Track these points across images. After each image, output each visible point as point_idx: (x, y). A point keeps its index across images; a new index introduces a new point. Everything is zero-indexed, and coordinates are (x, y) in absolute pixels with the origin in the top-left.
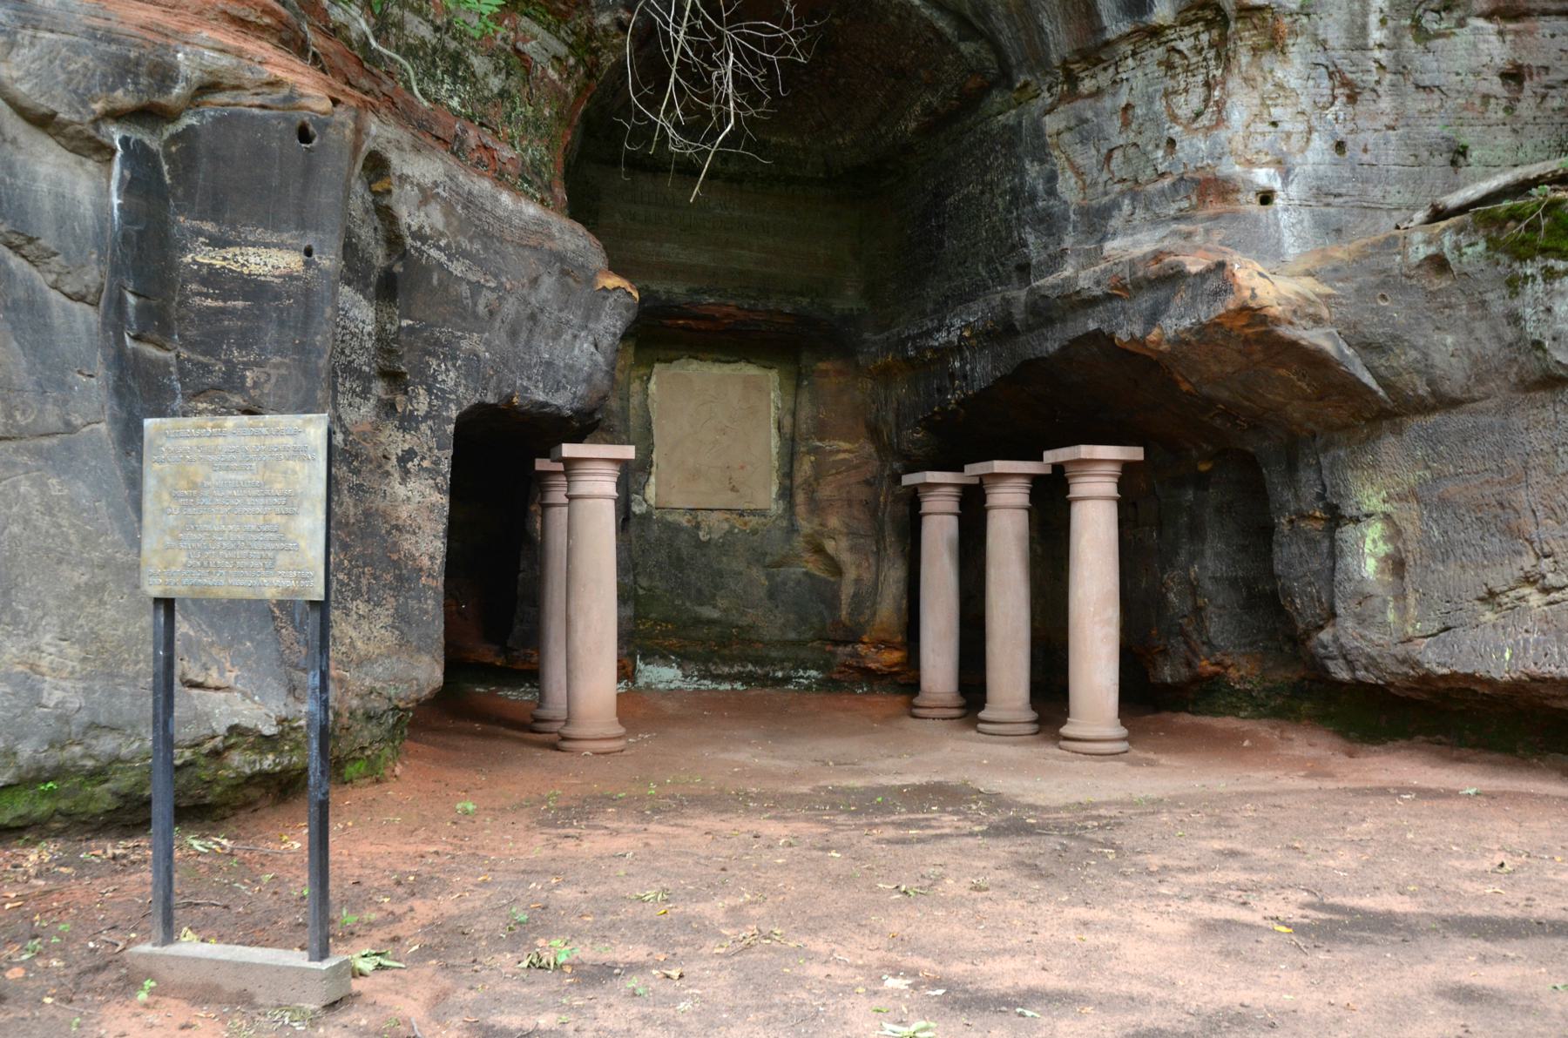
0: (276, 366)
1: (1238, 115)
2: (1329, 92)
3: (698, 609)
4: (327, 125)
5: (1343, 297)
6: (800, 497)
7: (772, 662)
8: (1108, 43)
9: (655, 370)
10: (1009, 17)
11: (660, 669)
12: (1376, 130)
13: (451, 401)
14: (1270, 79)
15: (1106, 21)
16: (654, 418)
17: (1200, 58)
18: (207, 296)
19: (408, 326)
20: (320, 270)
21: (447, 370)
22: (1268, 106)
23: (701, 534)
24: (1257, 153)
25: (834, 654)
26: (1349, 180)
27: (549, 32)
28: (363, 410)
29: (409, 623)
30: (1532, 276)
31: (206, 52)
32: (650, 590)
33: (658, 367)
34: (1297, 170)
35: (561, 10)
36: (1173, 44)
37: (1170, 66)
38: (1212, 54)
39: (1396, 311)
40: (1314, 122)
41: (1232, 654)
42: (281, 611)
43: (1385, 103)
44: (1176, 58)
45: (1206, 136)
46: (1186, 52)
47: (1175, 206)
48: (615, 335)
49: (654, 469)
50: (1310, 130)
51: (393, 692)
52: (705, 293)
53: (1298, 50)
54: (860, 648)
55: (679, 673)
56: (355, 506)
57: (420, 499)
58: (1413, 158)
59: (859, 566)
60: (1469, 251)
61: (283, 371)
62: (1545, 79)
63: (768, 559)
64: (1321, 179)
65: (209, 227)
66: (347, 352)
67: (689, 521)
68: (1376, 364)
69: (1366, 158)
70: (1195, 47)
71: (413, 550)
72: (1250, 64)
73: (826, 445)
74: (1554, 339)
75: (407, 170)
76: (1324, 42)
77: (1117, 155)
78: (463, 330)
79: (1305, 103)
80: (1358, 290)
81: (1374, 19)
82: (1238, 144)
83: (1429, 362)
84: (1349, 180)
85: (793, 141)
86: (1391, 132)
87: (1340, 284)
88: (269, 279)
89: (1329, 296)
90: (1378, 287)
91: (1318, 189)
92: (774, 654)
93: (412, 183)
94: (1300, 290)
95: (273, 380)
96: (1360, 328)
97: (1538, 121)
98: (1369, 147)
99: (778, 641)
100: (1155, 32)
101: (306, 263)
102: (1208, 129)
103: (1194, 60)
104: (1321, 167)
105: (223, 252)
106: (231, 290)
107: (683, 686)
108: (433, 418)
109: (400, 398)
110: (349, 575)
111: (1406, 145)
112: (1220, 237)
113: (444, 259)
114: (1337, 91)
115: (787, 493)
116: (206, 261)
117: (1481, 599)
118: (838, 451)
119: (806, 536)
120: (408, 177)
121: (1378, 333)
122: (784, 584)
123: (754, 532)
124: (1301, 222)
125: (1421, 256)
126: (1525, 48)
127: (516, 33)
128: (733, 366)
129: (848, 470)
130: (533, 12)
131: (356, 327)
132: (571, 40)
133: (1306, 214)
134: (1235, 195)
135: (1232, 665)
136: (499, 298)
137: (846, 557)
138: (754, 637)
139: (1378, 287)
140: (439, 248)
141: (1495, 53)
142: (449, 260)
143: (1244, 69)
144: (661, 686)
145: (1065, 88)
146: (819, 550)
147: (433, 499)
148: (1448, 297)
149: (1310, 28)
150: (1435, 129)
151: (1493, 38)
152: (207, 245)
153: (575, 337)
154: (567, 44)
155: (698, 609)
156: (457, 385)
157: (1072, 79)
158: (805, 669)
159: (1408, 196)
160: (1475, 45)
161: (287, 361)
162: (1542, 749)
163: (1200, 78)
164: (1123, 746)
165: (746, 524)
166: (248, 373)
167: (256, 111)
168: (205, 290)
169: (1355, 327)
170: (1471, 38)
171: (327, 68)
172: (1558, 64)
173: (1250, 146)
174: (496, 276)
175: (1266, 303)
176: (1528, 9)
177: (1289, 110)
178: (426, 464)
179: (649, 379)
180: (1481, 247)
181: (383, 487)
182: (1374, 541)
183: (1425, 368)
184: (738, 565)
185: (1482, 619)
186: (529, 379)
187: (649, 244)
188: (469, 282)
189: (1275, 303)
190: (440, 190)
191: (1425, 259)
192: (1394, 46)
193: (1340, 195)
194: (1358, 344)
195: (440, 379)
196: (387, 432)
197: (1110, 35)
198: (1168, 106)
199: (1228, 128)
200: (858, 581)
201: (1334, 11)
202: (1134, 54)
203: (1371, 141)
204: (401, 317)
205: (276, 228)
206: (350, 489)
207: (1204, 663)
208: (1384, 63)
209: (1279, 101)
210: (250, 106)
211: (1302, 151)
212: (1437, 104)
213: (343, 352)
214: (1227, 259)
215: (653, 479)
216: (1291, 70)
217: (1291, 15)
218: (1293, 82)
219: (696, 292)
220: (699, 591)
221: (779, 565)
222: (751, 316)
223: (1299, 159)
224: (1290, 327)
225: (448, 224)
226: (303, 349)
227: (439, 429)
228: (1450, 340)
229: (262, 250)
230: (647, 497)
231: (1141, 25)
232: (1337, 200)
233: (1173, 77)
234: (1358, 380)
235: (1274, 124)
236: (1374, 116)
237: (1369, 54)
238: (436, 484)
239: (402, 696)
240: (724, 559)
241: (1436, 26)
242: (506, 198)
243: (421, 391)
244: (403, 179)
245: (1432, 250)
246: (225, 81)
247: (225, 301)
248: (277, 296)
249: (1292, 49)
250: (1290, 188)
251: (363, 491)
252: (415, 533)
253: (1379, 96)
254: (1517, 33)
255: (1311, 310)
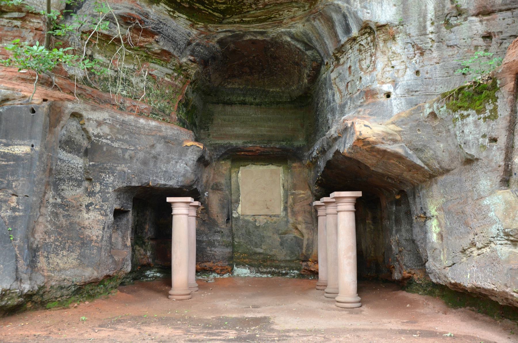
0: (22, 181)
1: (380, 66)
2: (413, 53)
3: (256, 249)
4: (39, 107)
5: (405, 131)
6: (289, 210)
7: (281, 267)
8: (343, 45)
9: (240, 169)
10: (317, 40)
11: (242, 270)
12: (431, 65)
13: (109, 186)
14: (390, 51)
15: (341, 38)
16: (240, 185)
17: (369, 47)
18: (3, 161)
19: (93, 164)
20: (35, 151)
21: (109, 177)
22: (391, 61)
23: (257, 223)
24: (386, 79)
25: (301, 265)
26: (420, 85)
27: (163, 66)
28: (78, 191)
29: (85, 258)
30: (458, 118)
31: (2, 90)
32: (239, 243)
33: (241, 168)
34: (400, 84)
35: (165, 60)
36: (360, 42)
37: (360, 51)
38: (371, 44)
39: (423, 135)
40: (408, 65)
41: (414, 269)
42: (20, 255)
43: (435, 54)
44: (362, 48)
45: (370, 75)
46: (364, 45)
47: (360, 101)
48: (194, 160)
49: (240, 202)
50: (406, 68)
51: (74, 280)
52: (249, 143)
53: (400, 38)
54: (309, 263)
55: (249, 271)
56: (66, 221)
57: (94, 218)
58: (446, 74)
59: (308, 234)
60: (442, 109)
61: (24, 182)
62: (501, 36)
63: (280, 232)
64: (409, 86)
65: (4, 141)
66: (70, 173)
67: (253, 219)
68: (421, 157)
69: (427, 76)
70: (367, 43)
71: (90, 234)
72: (383, 46)
73: (296, 192)
74: (465, 144)
75: (90, 116)
76: (409, 34)
77: (349, 84)
78: (118, 164)
79: (404, 58)
80: (410, 128)
81: (428, 23)
82: (379, 77)
83: (436, 155)
84: (420, 85)
85: (278, 90)
86: (437, 65)
87: (404, 126)
88: (21, 155)
89: (400, 131)
90: (416, 126)
91: (408, 90)
92: (282, 265)
93: (93, 120)
94: (384, 130)
95: (21, 185)
96: (412, 143)
97: (498, 53)
98: (428, 72)
99: (284, 260)
100: (354, 39)
101: (32, 150)
102: (371, 72)
103: (367, 47)
104: (410, 81)
105: (8, 148)
106: (10, 159)
107: (250, 275)
108: (101, 192)
109: (91, 186)
110: (61, 243)
111: (444, 69)
112: (368, 112)
113: (109, 142)
114: (416, 52)
115: (285, 209)
116: (3, 151)
117: (461, 252)
118: (300, 194)
119: (292, 224)
120: (91, 118)
121: (419, 145)
122: (287, 240)
123: (275, 223)
124: (401, 103)
125: (428, 113)
126: (491, 25)
127: (149, 68)
128: (267, 166)
129: (304, 200)
130: (155, 61)
131: (75, 165)
132: (173, 68)
133: (403, 100)
134: (376, 96)
135: (414, 273)
136: (135, 152)
137: (304, 231)
138: (275, 259)
139: (416, 126)
140: (107, 139)
141: (479, 29)
142: (112, 142)
143: (381, 48)
144: (242, 275)
145: (336, 62)
146: (297, 228)
147: (99, 218)
148: (439, 128)
149: (404, 30)
150: (455, 62)
151: (478, 23)
152: (3, 146)
153: (177, 162)
154: (172, 69)
155: (256, 249)
156: (113, 181)
157: (338, 59)
158: (293, 270)
159: (445, 88)
160: (470, 27)
161: (25, 179)
162: (503, 317)
163: (369, 53)
164: (359, 304)
165: (272, 220)
166: (13, 183)
167: (19, 106)
168: (2, 159)
169: (411, 143)
170: (469, 25)
171: (60, 89)
172: (506, 30)
173: (384, 76)
174: (134, 146)
175: (366, 136)
176: (493, 10)
177: (398, 61)
178: (97, 207)
179: (238, 172)
180: (445, 108)
181: (79, 215)
182: (435, 226)
183: (435, 157)
184: (270, 234)
185: (462, 260)
186: (156, 177)
187: (230, 128)
188: (121, 149)
189: (372, 136)
190: (108, 121)
191: (429, 114)
192: (438, 32)
193: (417, 91)
194: (413, 149)
195: (106, 180)
196: (83, 198)
197: (342, 42)
198: (360, 65)
199: (376, 71)
200: (308, 239)
201: (413, 22)
202: (351, 48)
203: (429, 69)
204: (90, 161)
205: (23, 140)
206: (63, 216)
207: (405, 272)
208: (434, 39)
209: (394, 58)
210: (18, 104)
211: (403, 76)
212: (456, 52)
213: (68, 174)
214: (437, 120)
215: (240, 205)
216: (398, 47)
217: (396, 26)
218: (399, 51)
219: (246, 143)
220: (256, 243)
221: (285, 233)
222: (266, 149)
223: (401, 79)
224: (382, 145)
225: (111, 131)
226: (29, 175)
227: (104, 195)
228: (442, 145)
229: (19, 147)
230: (238, 211)
231: (350, 38)
232: (416, 93)
233: (361, 54)
234: (415, 164)
235: (393, 67)
236: (430, 59)
237: (427, 36)
238: (101, 213)
239: (78, 281)
240: (265, 232)
241: (455, 22)
242: (142, 121)
243: (98, 184)
244: (89, 119)
245: (431, 110)
246: (10, 98)
247: (8, 162)
248: (23, 160)
249: (398, 39)
250: (397, 91)
251: (70, 216)
252: (90, 229)
253: (432, 52)
254: (488, 20)
255: (391, 137)
